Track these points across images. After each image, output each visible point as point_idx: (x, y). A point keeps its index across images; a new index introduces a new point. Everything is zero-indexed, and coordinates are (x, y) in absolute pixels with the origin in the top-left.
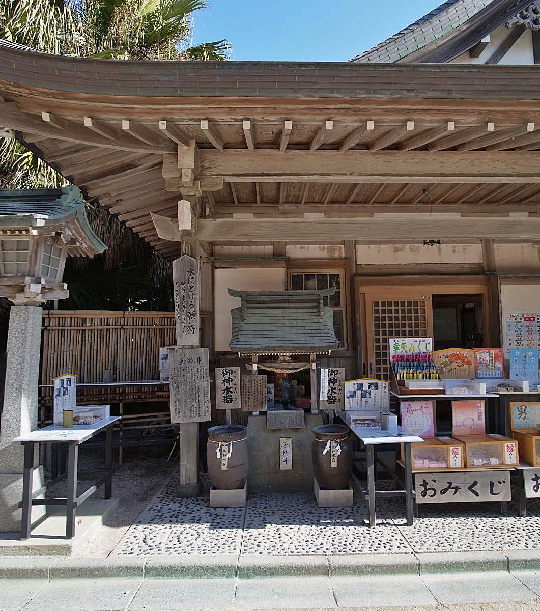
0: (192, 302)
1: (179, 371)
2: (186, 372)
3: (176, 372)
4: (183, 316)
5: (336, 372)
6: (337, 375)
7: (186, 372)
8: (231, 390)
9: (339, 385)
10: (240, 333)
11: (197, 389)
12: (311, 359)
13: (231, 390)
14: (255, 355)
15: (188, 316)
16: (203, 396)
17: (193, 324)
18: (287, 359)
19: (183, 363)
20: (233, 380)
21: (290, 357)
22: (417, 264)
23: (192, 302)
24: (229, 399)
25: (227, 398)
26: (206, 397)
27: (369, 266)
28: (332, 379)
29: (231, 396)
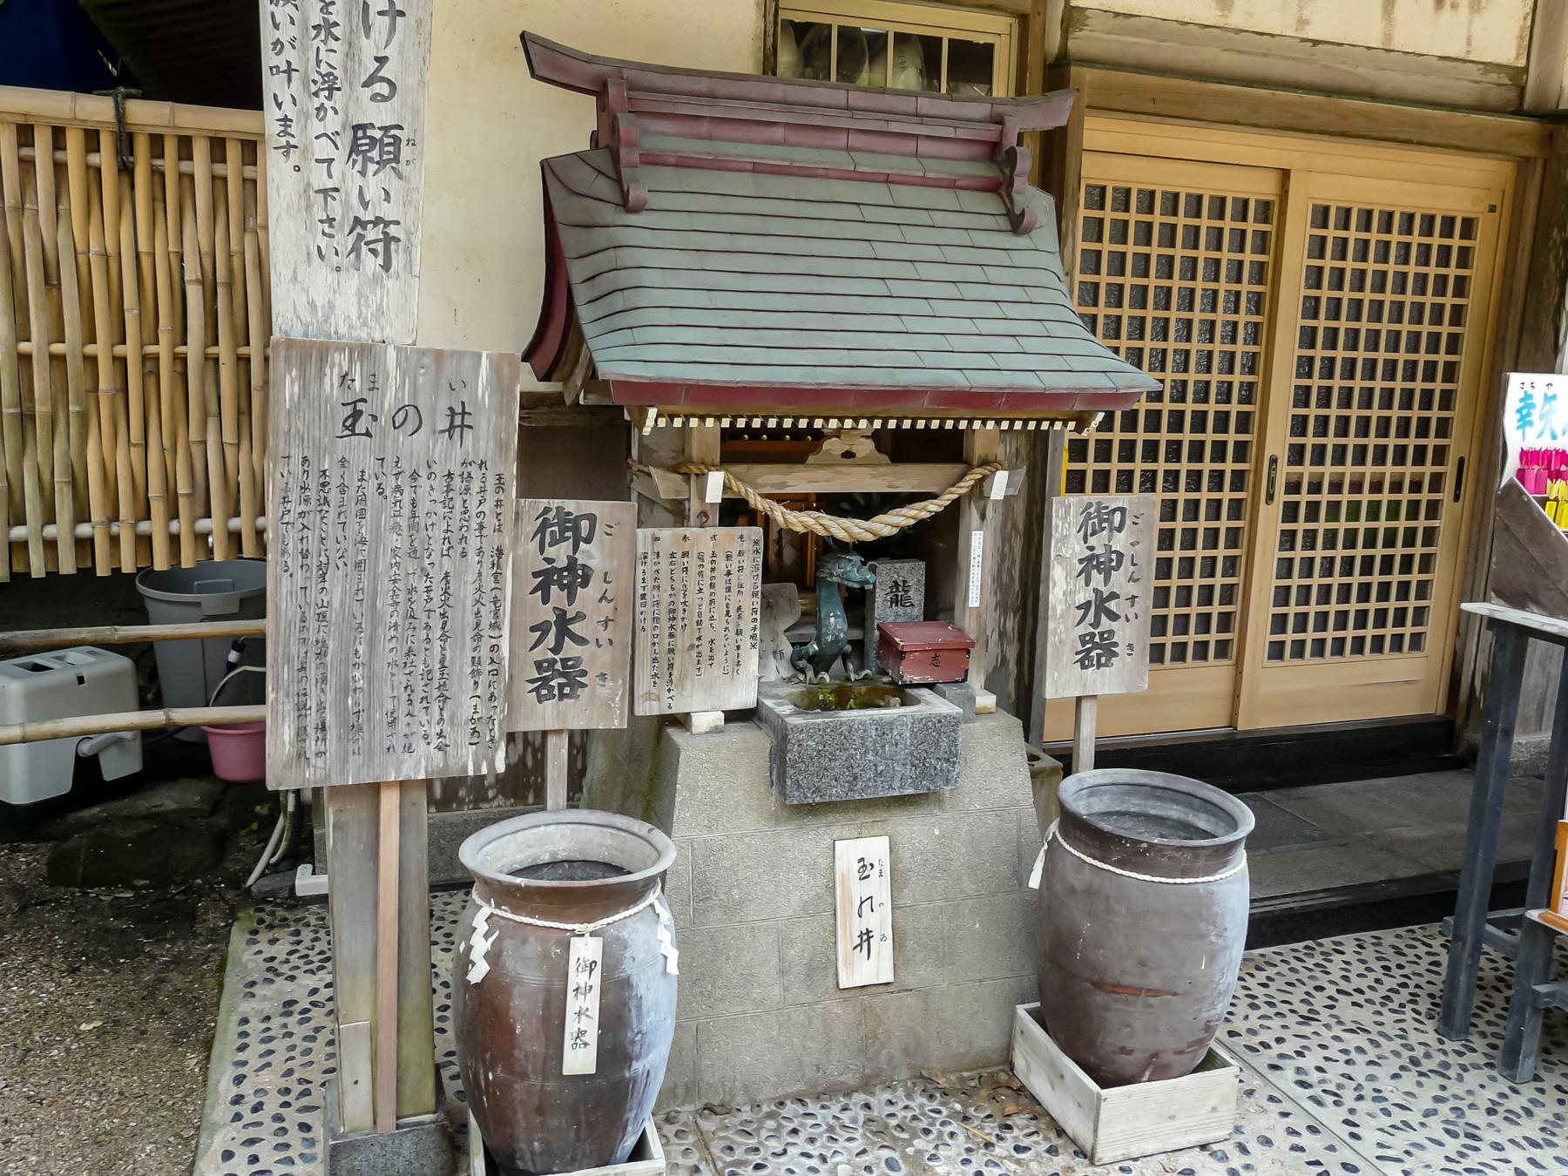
0: (381, 60)
1: (335, 481)
2: (380, 489)
3: (313, 484)
4: (323, 149)
5: (585, 524)
6: (588, 540)
7: (380, 489)
8: (1112, 605)
9: (603, 598)
10: (624, 278)
11: (437, 594)
12: (695, 450)
13: (1112, 605)
14: (991, 425)
15: (354, 149)
16: (469, 633)
17: (387, 211)
18: (865, 448)
19: (361, 427)
20: (1127, 560)
21: (876, 436)
22: (1304, 40)
23: (381, 60)
24: (1096, 651)
25: (1096, 646)
26: (486, 643)
27: (1120, 19)
28: (562, 562)
29: (1111, 632)
